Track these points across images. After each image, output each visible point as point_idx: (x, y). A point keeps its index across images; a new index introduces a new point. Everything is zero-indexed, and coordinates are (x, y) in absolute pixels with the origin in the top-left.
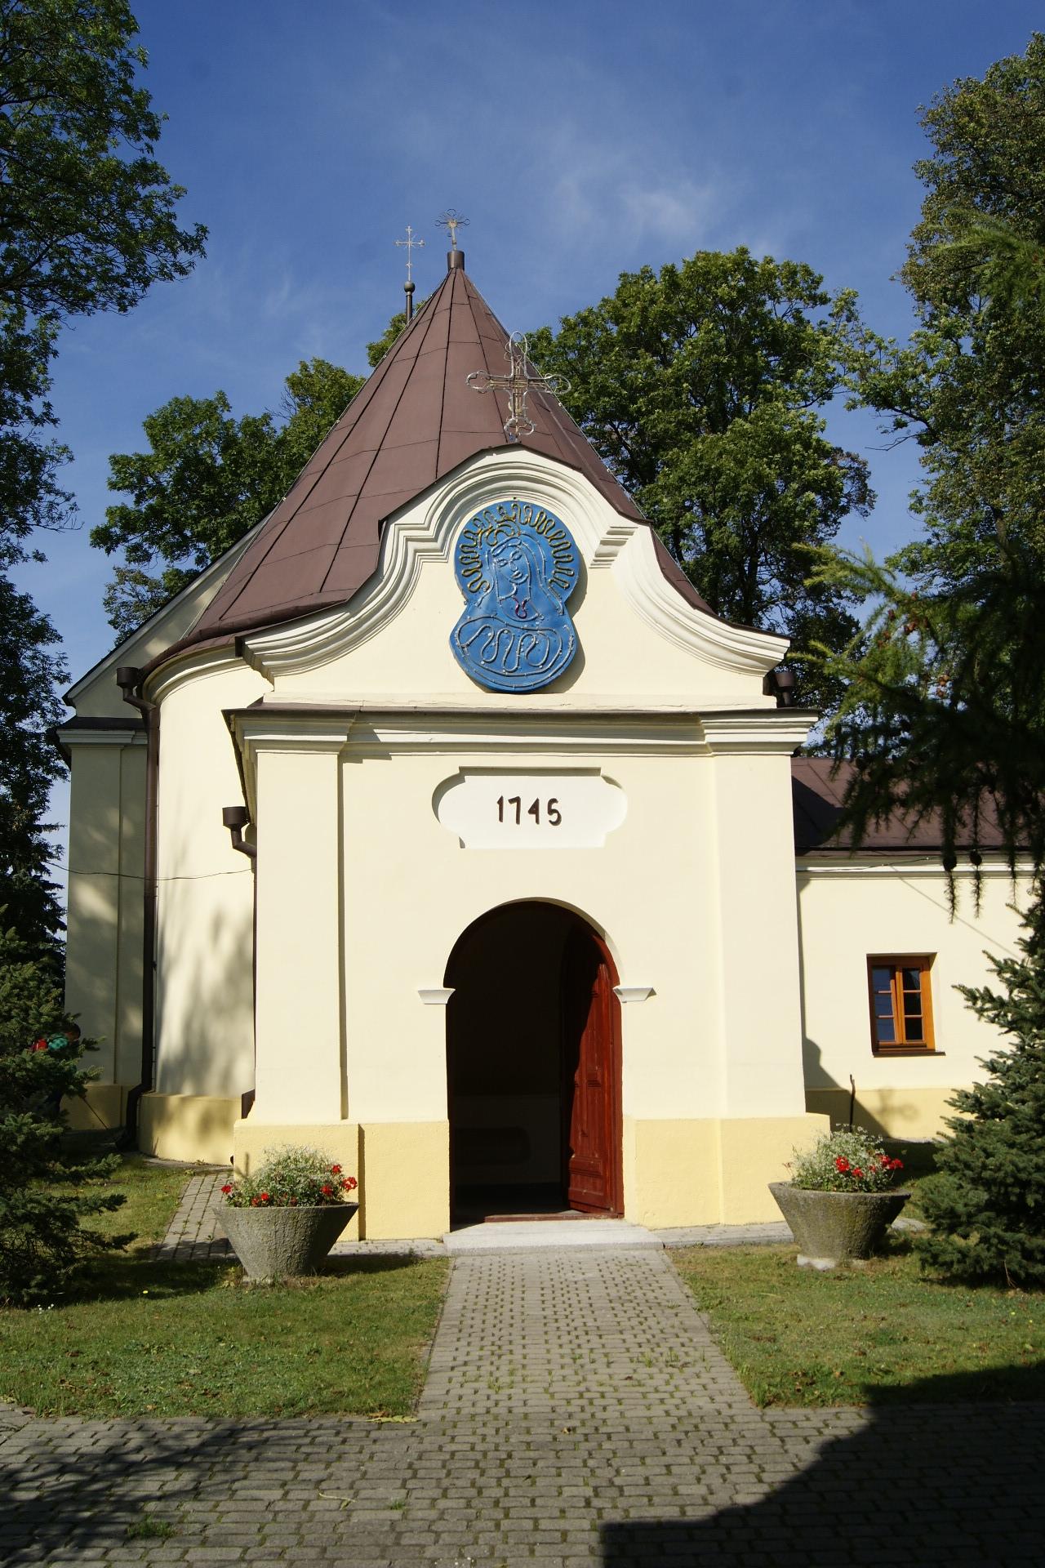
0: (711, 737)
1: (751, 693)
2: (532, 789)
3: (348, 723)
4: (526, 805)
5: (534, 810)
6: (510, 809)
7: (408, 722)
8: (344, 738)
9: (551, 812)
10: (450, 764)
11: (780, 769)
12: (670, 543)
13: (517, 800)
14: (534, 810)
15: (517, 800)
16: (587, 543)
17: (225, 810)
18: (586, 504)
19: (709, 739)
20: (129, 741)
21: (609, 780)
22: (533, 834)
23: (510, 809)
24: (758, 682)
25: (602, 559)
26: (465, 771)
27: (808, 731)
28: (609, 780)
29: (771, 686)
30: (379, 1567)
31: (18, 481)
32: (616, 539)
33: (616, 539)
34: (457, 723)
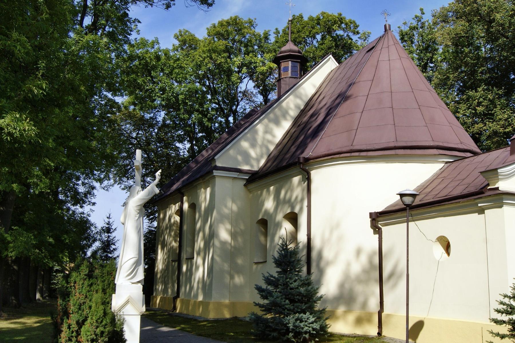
17: (371, 214)
20: (236, 176)
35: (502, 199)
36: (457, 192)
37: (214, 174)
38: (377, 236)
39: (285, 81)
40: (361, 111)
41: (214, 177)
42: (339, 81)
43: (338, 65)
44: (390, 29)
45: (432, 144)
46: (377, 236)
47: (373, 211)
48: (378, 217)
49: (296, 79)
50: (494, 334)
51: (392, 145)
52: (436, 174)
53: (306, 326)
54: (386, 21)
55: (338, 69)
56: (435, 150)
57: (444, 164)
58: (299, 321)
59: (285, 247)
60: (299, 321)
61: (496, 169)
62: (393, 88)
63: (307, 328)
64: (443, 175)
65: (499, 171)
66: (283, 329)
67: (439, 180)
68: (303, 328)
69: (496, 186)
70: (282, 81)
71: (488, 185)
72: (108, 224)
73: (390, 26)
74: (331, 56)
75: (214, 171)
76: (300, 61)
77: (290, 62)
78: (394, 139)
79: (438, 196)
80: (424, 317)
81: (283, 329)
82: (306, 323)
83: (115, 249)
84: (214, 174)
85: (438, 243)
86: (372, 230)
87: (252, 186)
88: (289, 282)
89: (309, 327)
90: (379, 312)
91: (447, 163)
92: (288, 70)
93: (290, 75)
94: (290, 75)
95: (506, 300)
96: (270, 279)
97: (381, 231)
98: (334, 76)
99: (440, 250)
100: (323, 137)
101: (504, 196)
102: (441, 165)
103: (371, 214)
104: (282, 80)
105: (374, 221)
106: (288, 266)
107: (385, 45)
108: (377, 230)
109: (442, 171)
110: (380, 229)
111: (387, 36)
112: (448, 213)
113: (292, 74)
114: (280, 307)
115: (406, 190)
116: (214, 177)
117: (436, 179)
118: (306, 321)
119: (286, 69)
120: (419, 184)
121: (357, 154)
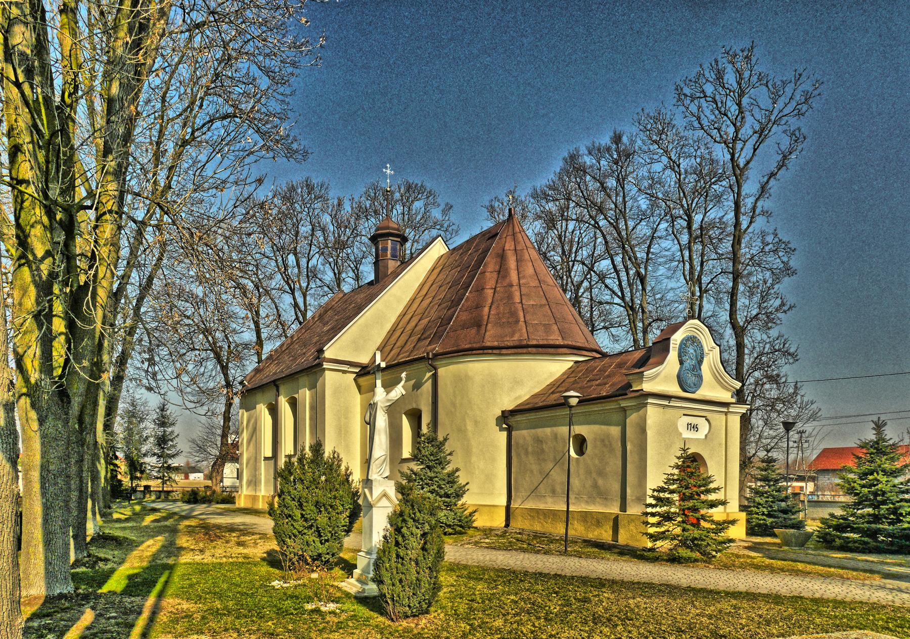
2: (694, 420)
37: (324, 366)
72: (163, 417)
76: (399, 240)
84: (324, 366)
91: (576, 362)
95: (656, 494)
116: (324, 369)
121: (490, 351)
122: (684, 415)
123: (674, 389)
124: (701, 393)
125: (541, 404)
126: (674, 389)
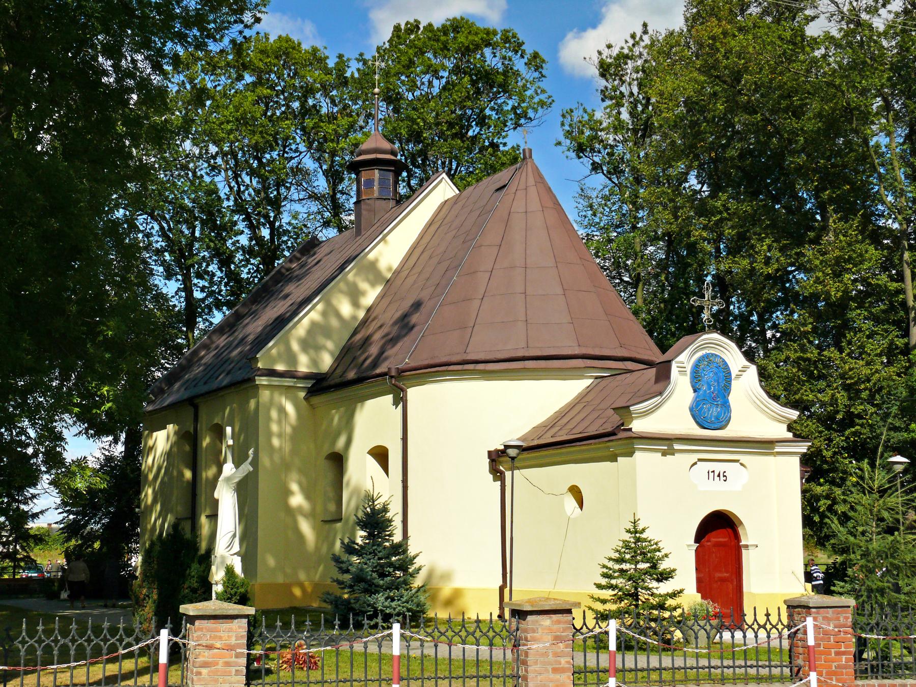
0: (777, 450)
1: (781, 432)
2: (719, 467)
3: (667, 442)
4: (716, 474)
5: (719, 476)
6: (711, 475)
7: (685, 442)
8: (666, 448)
9: (724, 476)
10: (694, 457)
11: (796, 461)
12: (763, 375)
13: (713, 472)
14: (719, 476)
15: (713, 472)
16: (734, 372)
17: (489, 452)
18: (732, 352)
19: (776, 450)
20: (291, 384)
21: (742, 464)
22: (718, 484)
23: (711, 475)
24: (785, 427)
25: (738, 376)
26: (700, 460)
27: (803, 448)
28: (742, 464)
29: (790, 428)
30: (874, 686)
31: (129, 166)
32: (743, 370)
33: (743, 370)
34: (701, 443)
35: (633, 444)
36: (592, 431)
38: (499, 483)
39: (369, 205)
40: (481, 297)
41: (257, 387)
42: (454, 232)
43: (458, 192)
44: (531, 157)
45: (577, 351)
46: (499, 483)
47: (492, 449)
48: (499, 456)
49: (386, 201)
50: (595, 599)
51: (520, 354)
52: (580, 394)
53: (400, 606)
54: (526, 143)
55: (455, 203)
56: (580, 360)
57: (592, 380)
58: (389, 600)
59: (370, 503)
60: (389, 600)
61: (628, 407)
62: (528, 261)
63: (400, 608)
64: (586, 399)
65: (632, 408)
66: (370, 611)
67: (581, 406)
68: (394, 609)
69: (630, 427)
70: (363, 206)
71: (623, 424)
73: (530, 151)
74: (444, 175)
75: (256, 378)
77: (376, 171)
78: (523, 345)
79: (575, 431)
80: (548, 590)
81: (370, 611)
82: (399, 602)
83: (34, 496)
85: (569, 494)
86: (491, 476)
87: (316, 400)
88: (376, 549)
89: (403, 607)
90: (500, 587)
91: (597, 378)
92: (374, 185)
93: (376, 195)
94: (376, 195)
96: (350, 547)
97: (505, 476)
98: (448, 217)
99: (570, 502)
100: (425, 334)
101: (635, 441)
102: (588, 382)
103: (489, 452)
104: (362, 202)
105: (494, 463)
106: (376, 528)
107: (522, 186)
108: (498, 474)
109: (589, 390)
110: (502, 473)
111: (525, 170)
112: (588, 456)
113: (380, 192)
114: (366, 582)
115: (510, 441)
117: (578, 403)
118: (398, 600)
119: (369, 183)
120: (557, 409)
121: (471, 367)
122: (700, 460)
123: (691, 428)
124: (726, 433)
125: (535, 443)
126: (691, 428)
